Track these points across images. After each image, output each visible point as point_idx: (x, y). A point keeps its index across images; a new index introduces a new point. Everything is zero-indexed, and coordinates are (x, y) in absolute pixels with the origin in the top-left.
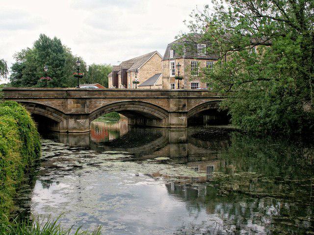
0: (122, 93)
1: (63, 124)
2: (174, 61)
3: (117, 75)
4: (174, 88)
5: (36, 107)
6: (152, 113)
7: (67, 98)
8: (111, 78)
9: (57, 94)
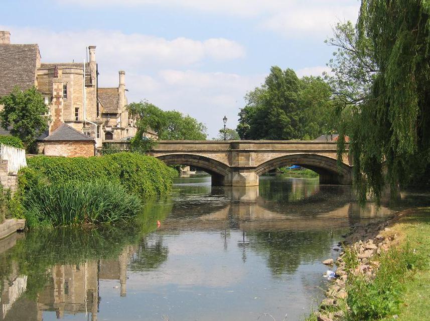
0: (293, 145)
1: (228, 177)
9: (221, 147)
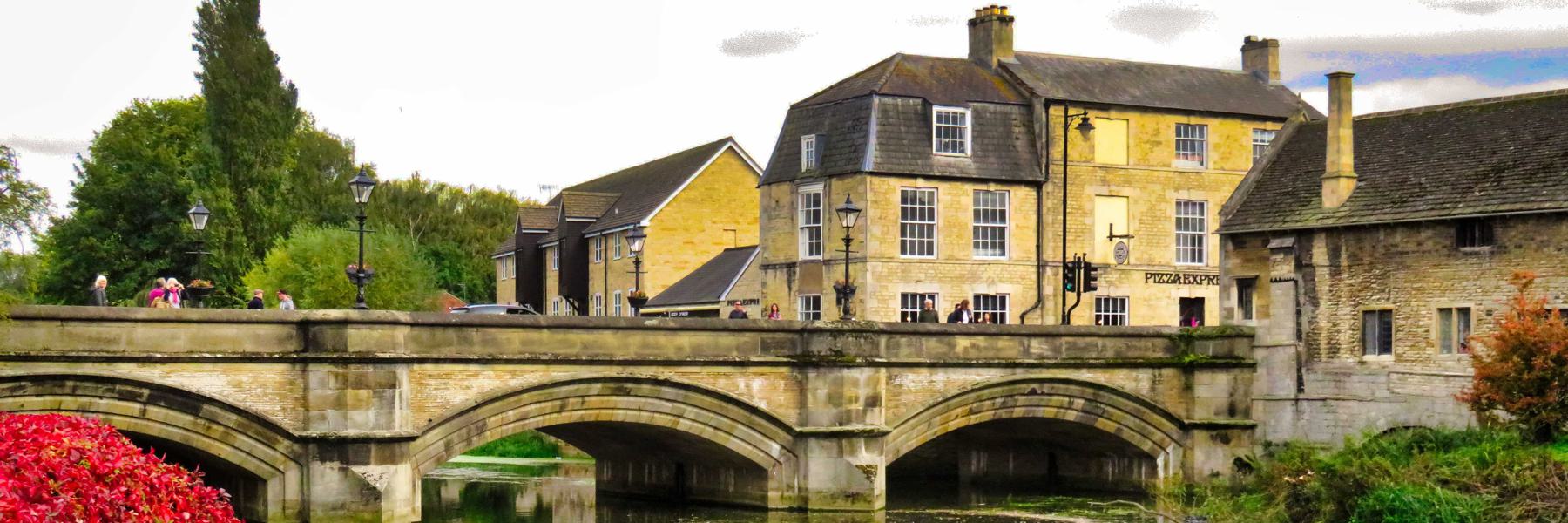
2: (818, 188)
3: (538, 256)
4: (817, 316)
5: (152, 401)
6: (721, 438)
7: (305, 361)
8: (511, 266)
